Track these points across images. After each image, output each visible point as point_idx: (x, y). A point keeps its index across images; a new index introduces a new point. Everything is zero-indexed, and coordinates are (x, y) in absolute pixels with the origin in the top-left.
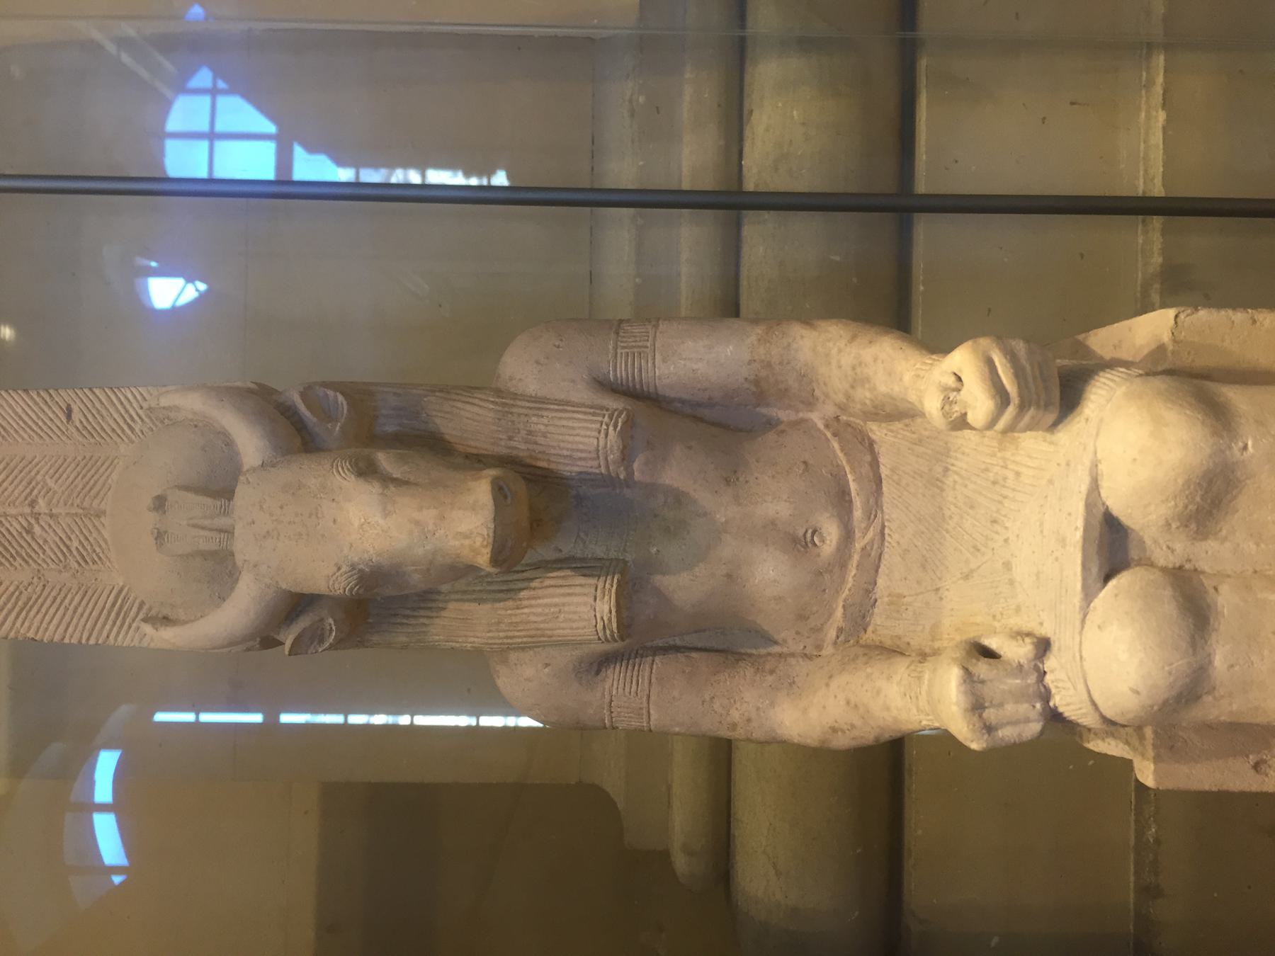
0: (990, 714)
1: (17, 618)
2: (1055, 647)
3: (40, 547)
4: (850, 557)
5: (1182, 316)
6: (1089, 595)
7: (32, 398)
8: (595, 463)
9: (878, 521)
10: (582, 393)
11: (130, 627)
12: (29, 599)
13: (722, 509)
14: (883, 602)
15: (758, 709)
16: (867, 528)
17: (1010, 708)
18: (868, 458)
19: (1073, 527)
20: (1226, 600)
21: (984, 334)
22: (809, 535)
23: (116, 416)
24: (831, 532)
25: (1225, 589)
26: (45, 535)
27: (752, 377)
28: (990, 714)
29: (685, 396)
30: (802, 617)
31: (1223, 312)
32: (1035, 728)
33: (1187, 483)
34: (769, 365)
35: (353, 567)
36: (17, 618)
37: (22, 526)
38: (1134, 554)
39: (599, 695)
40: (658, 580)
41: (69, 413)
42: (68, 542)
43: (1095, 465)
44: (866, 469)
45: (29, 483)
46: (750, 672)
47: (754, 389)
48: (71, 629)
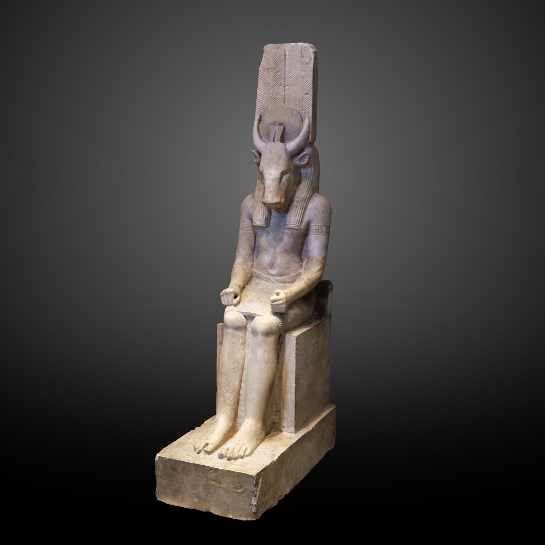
0: (225, 296)
6: (242, 313)
10: (306, 218)
13: (279, 249)
14: (260, 282)
19: (253, 312)
20: (240, 334)
24: (274, 272)
25: (242, 335)
28: (225, 296)
32: (223, 303)
38: (249, 321)
40: (264, 235)
41: (307, 94)
44: (287, 280)
46: (249, 253)
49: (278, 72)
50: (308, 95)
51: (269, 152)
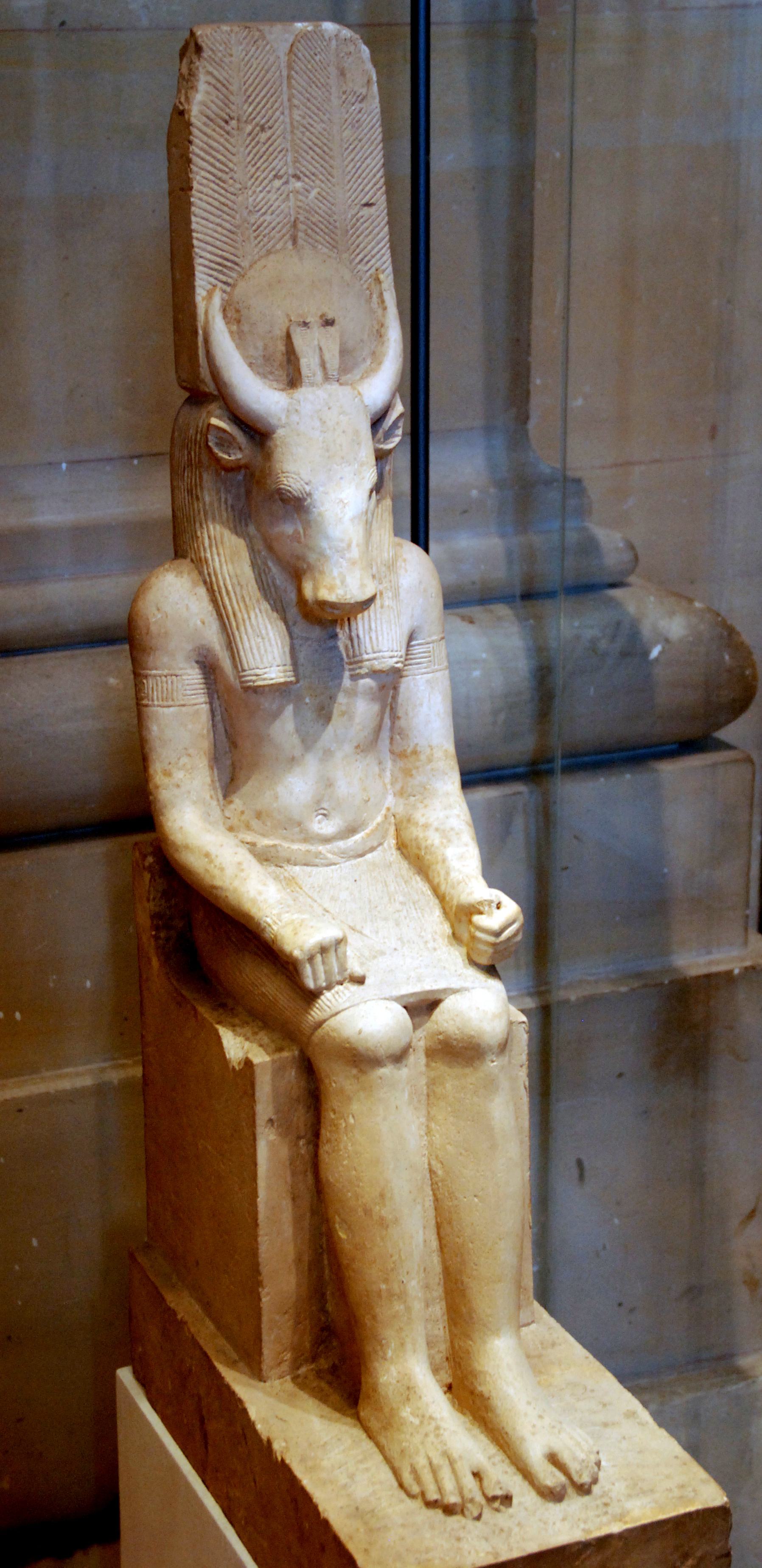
0: (319, 958)
1: (209, 172)
2: (362, 987)
3: (264, 188)
4: (312, 844)
5: (524, 1025)
6: (397, 999)
7: (378, 171)
8: (369, 650)
9: (339, 860)
11: (211, 276)
12: (224, 182)
15: (189, 792)
16: (334, 853)
17: (321, 969)
18: (375, 844)
21: (524, 916)
22: (322, 811)
23: (369, 247)
24: (327, 827)
26: (274, 190)
27: (419, 749)
29: (401, 699)
30: (259, 815)
31: (526, 1048)
32: (310, 984)
33: (472, 1037)
34: (430, 760)
35: (309, 495)
36: (209, 172)
37: (280, 170)
39: (181, 665)
40: (289, 709)
41: (368, 205)
42: (270, 212)
43: (467, 989)
44: (369, 844)
45: (313, 174)
47: (409, 751)
48: (204, 222)
49: (263, 129)
50: (372, 210)
51: (317, 424)
